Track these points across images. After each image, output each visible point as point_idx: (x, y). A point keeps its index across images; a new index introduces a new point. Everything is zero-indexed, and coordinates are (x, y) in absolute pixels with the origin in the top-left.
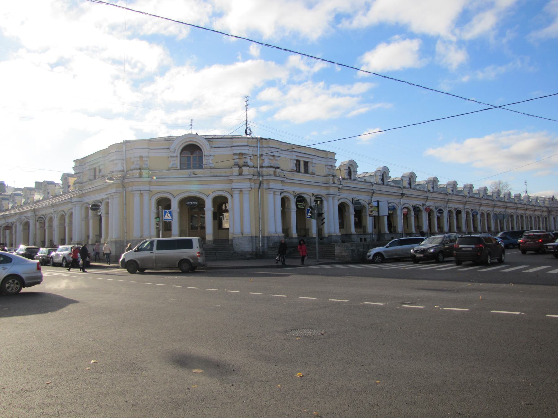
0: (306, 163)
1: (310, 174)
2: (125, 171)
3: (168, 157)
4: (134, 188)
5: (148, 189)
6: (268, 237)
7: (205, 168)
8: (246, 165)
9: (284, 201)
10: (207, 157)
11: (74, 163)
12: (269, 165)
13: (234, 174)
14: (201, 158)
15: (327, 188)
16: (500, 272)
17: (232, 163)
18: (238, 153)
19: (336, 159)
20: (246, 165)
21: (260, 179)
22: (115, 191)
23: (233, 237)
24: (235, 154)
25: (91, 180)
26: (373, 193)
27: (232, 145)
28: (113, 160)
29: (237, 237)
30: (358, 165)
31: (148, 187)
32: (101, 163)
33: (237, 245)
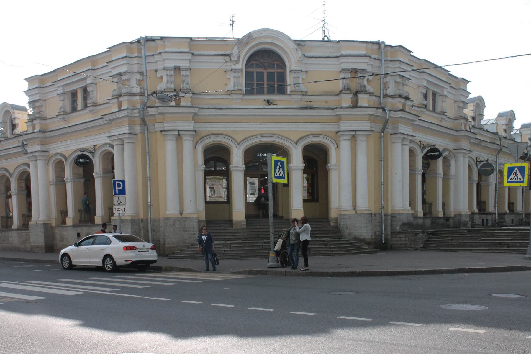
0: (434, 94)
1: (437, 113)
2: (146, 95)
3: (225, 71)
4: (167, 126)
5: (191, 128)
6: (393, 216)
7: (292, 93)
8: (364, 91)
9: (59, 166)
10: (295, 73)
11: (26, 84)
12: (398, 92)
13: (344, 105)
14: (282, 77)
15: (456, 139)
16: (484, 304)
17: (340, 85)
18: (350, 68)
19: (468, 91)
20: (364, 91)
21: (386, 117)
22: (127, 131)
23: (341, 215)
24: (344, 70)
25: (65, 113)
26: (499, 151)
27: (338, 54)
28: (120, 74)
29: (347, 215)
30: (486, 106)
31: (193, 124)
32: (89, 81)
33: (347, 228)
